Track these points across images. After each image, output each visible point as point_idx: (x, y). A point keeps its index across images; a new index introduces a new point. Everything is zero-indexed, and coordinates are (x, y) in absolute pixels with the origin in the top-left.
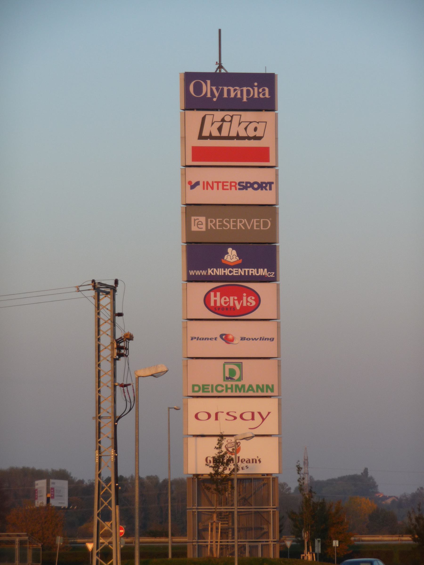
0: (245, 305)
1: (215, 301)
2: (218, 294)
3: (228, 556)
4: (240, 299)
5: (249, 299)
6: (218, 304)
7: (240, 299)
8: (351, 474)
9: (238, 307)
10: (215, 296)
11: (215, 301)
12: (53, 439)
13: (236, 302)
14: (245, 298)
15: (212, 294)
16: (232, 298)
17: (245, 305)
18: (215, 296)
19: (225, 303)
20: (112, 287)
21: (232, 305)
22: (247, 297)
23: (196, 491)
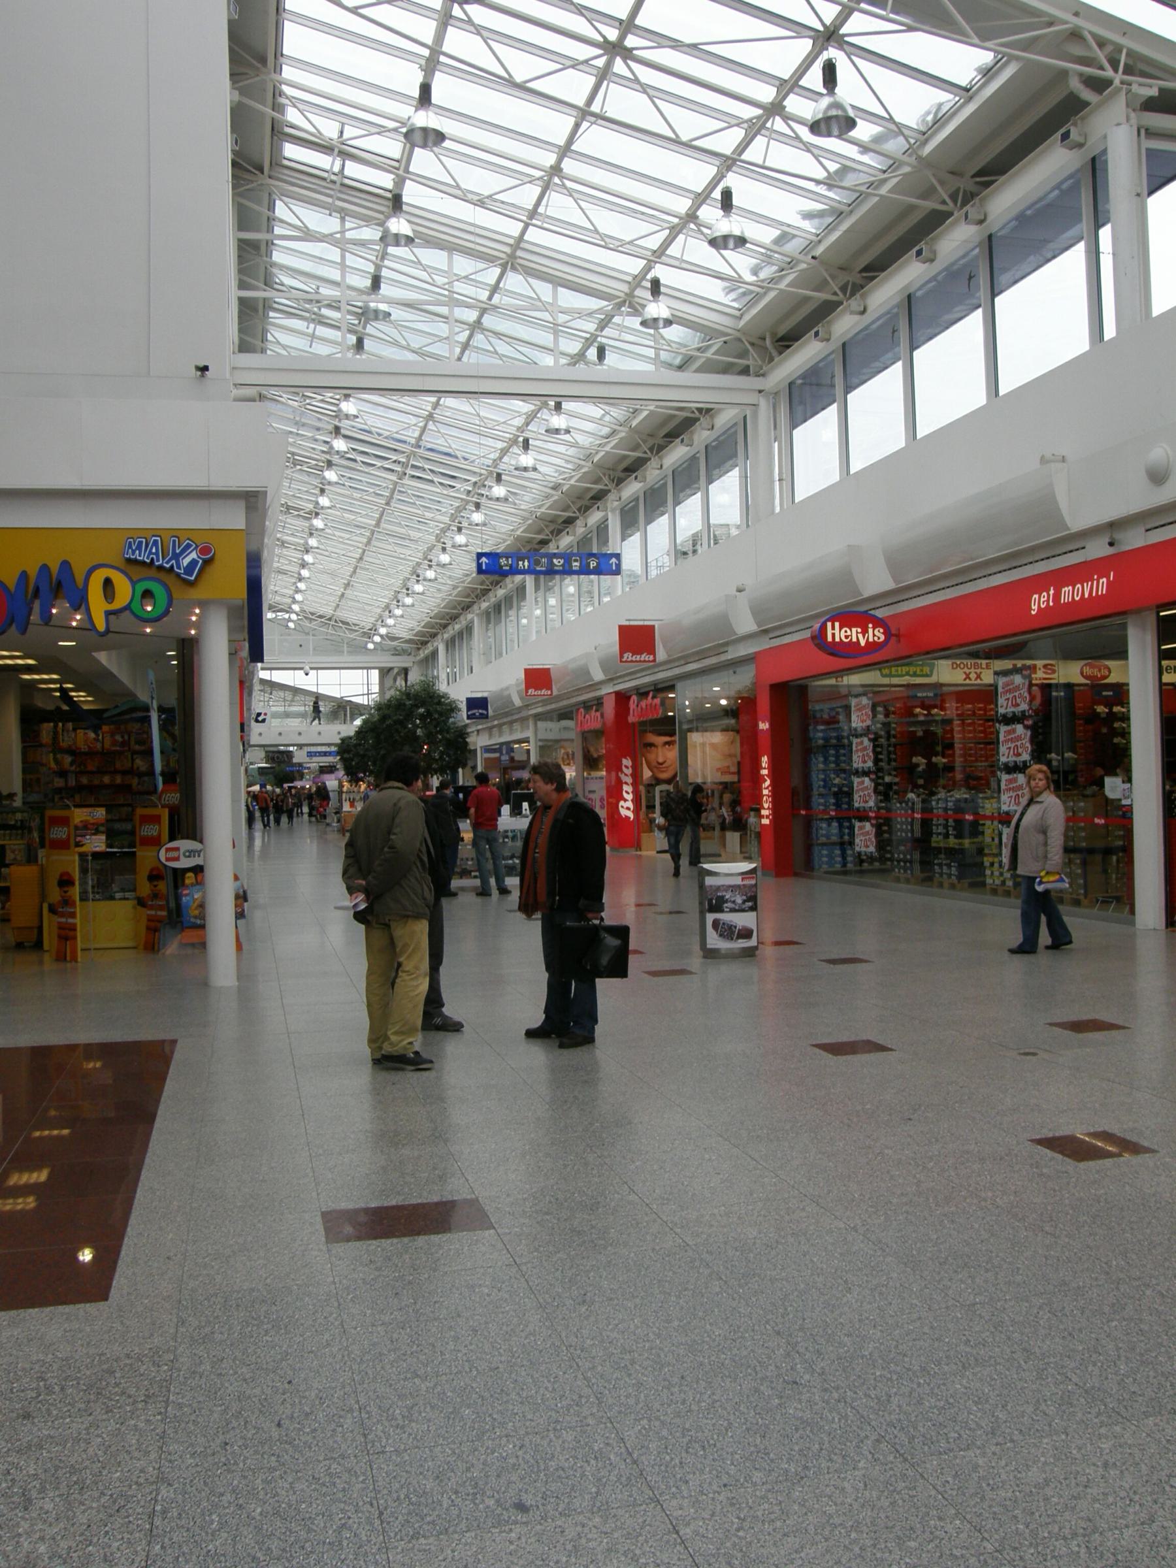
0: (871, 640)
1: (833, 635)
2: (837, 624)
3: (765, 821)
4: (865, 632)
5: (876, 632)
6: (837, 639)
7: (865, 632)
8: (619, 979)
9: (863, 643)
10: (833, 628)
11: (833, 635)
12: (279, 9)
13: (860, 636)
14: (870, 631)
15: (829, 624)
16: (854, 630)
17: (871, 640)
18: (833, 628)
19: (847, 637)
20: (639, 32)
21: (854, 639)
22: (874, 628)
23: (1016, 37)
